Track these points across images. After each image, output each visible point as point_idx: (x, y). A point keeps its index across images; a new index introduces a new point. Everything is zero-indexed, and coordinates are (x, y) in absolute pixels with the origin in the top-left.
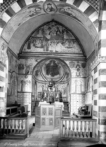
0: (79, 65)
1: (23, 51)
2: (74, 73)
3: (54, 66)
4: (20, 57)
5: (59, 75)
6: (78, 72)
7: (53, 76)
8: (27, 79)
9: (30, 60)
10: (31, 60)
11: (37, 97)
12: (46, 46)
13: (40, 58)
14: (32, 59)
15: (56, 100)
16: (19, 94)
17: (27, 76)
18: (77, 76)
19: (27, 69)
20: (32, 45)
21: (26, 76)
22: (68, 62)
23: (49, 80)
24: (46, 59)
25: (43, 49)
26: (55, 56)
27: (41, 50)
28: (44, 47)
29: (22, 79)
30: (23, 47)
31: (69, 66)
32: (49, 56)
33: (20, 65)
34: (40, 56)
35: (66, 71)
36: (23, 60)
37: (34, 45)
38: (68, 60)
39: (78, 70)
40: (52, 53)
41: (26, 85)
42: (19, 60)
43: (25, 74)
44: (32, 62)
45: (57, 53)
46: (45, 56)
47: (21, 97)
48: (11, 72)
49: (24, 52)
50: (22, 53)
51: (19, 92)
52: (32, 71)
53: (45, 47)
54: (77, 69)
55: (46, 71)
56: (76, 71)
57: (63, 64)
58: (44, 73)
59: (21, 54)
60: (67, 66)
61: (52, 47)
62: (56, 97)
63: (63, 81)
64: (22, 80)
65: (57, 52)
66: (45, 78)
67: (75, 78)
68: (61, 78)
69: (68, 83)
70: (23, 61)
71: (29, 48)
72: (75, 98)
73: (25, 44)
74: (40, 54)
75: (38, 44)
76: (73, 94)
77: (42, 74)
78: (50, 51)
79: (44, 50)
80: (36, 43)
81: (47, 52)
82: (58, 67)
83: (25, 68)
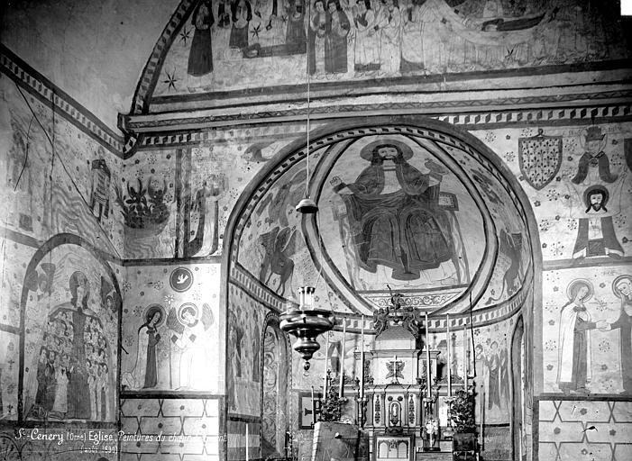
0: (602, 156)
1: (161, 89)
2: (563, 225)
3: (409, 201)
4: (139, 140)
5: (456, 263)
6: (596, 219)
7: (409, 274)
8: (186, 297)
9: (206, 152)
10: (217, 149)
11: (295, 427)
12: (329, 32)
13: (281, 129)
14: (221, 141)
15: (427, 450)
16: (130, 406)
17: (186, 272)
18: (583, 252)
19: (186, 221)
20: (220, 38)
21: (177, 273)
22: (504, 144)
23: (381, 302)
24: (335, 135)
25: (305, 58)
26: (400, 99)
27: (291, 70)
28: (313, 46)
29: (153, 297)
30: (161, 63)
31: (514, 168)
32: (351, 108)
33: (136, 195)
34: (283, 114)
35: (500, 224)
36: (159, 155)
37: (239, 40)
38: (509, 124)
39: (596, 199)
40: (374, 82)
41: (183, 341)
42: (130, 161)
43: (176, 260)
44: (228, 164)
45: (418, 80)
46: (312, 111)
47: (146, 427)
48: (31, 242)
49: (165, 99)
50: (153, 108)
51: (133, 396)
52: (222, 231)
53: (320, 42)
54: (582, 188)
55: (356, 240)
56: (579, 211)
57: (472, 165)
58: (341, 252)
59: (145, 111)
60: (504, 175)
61: (377, 34)
62: (431, 428)
63: (481, 304)
64: (156, 302)
65: (411, 75)
66: (352, 289)
67: (574, 264)
68: (472, 285)
69: (520, 318)
70: (157, 164)
71: (202, 62)
72: (570, 432)
73: (173, 38)
74: (279, 97)
75: (269, 27)
76: (553, 397)
77: (329, 260)
78: (358, 68)
79: (312, 70)
80: (254, 23)
81: (332, 78)
82: (443, 201)
83: (173, 217)
